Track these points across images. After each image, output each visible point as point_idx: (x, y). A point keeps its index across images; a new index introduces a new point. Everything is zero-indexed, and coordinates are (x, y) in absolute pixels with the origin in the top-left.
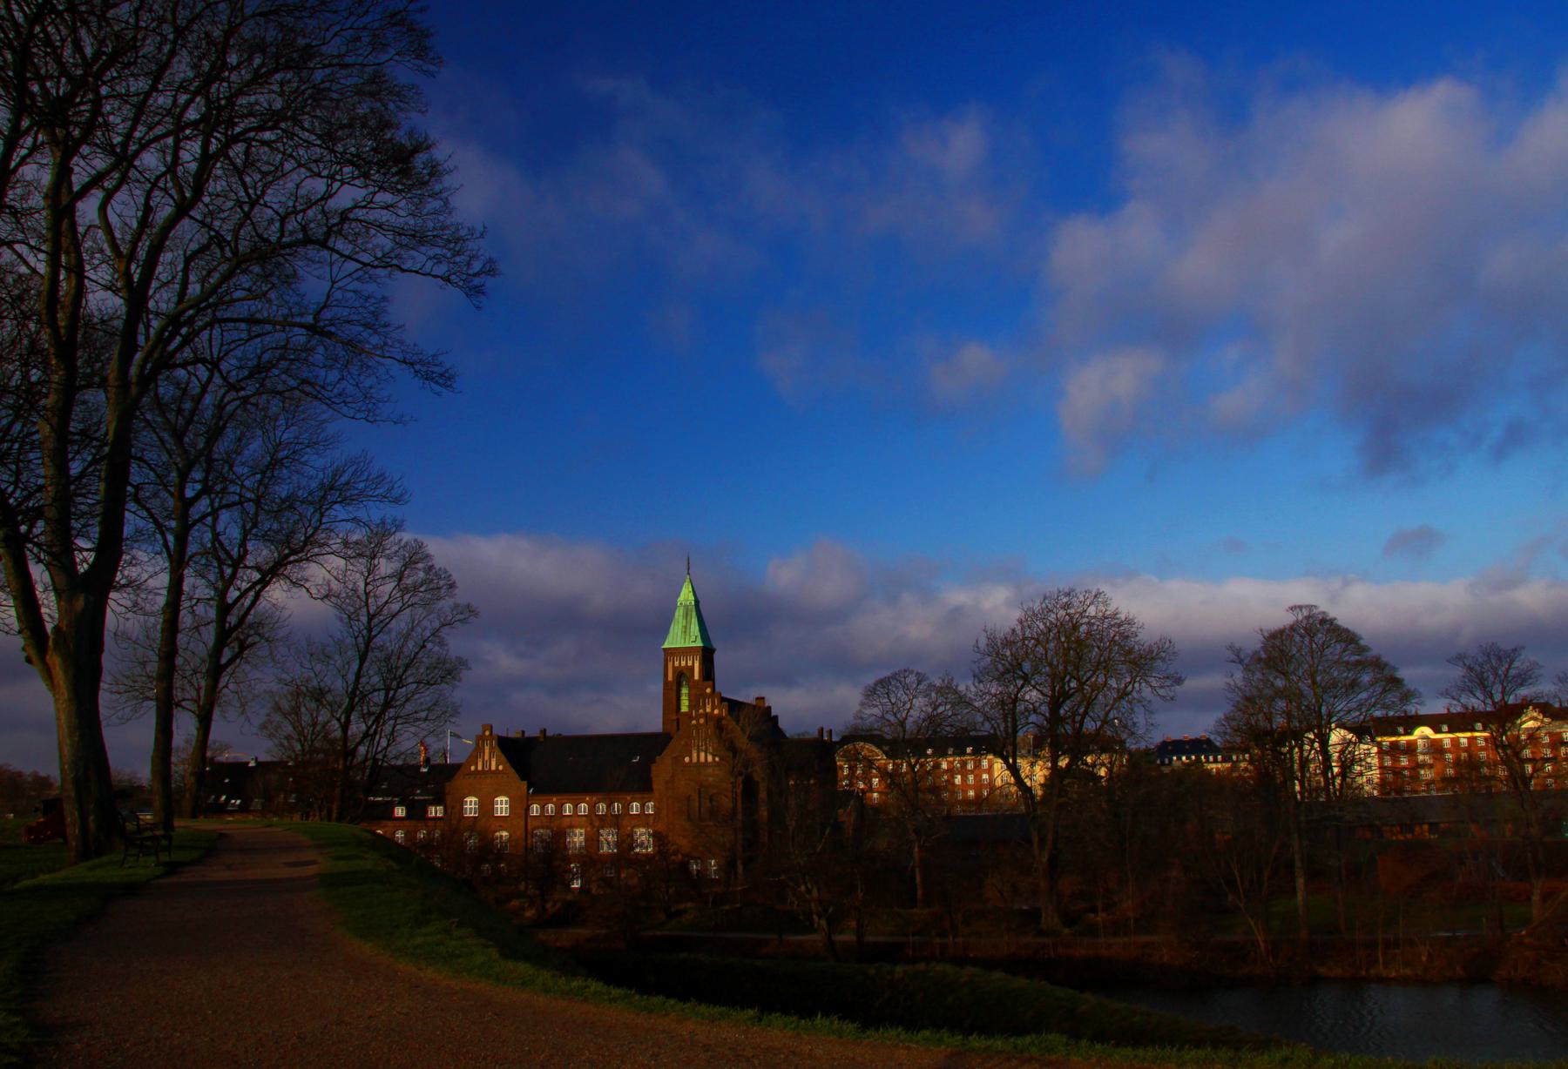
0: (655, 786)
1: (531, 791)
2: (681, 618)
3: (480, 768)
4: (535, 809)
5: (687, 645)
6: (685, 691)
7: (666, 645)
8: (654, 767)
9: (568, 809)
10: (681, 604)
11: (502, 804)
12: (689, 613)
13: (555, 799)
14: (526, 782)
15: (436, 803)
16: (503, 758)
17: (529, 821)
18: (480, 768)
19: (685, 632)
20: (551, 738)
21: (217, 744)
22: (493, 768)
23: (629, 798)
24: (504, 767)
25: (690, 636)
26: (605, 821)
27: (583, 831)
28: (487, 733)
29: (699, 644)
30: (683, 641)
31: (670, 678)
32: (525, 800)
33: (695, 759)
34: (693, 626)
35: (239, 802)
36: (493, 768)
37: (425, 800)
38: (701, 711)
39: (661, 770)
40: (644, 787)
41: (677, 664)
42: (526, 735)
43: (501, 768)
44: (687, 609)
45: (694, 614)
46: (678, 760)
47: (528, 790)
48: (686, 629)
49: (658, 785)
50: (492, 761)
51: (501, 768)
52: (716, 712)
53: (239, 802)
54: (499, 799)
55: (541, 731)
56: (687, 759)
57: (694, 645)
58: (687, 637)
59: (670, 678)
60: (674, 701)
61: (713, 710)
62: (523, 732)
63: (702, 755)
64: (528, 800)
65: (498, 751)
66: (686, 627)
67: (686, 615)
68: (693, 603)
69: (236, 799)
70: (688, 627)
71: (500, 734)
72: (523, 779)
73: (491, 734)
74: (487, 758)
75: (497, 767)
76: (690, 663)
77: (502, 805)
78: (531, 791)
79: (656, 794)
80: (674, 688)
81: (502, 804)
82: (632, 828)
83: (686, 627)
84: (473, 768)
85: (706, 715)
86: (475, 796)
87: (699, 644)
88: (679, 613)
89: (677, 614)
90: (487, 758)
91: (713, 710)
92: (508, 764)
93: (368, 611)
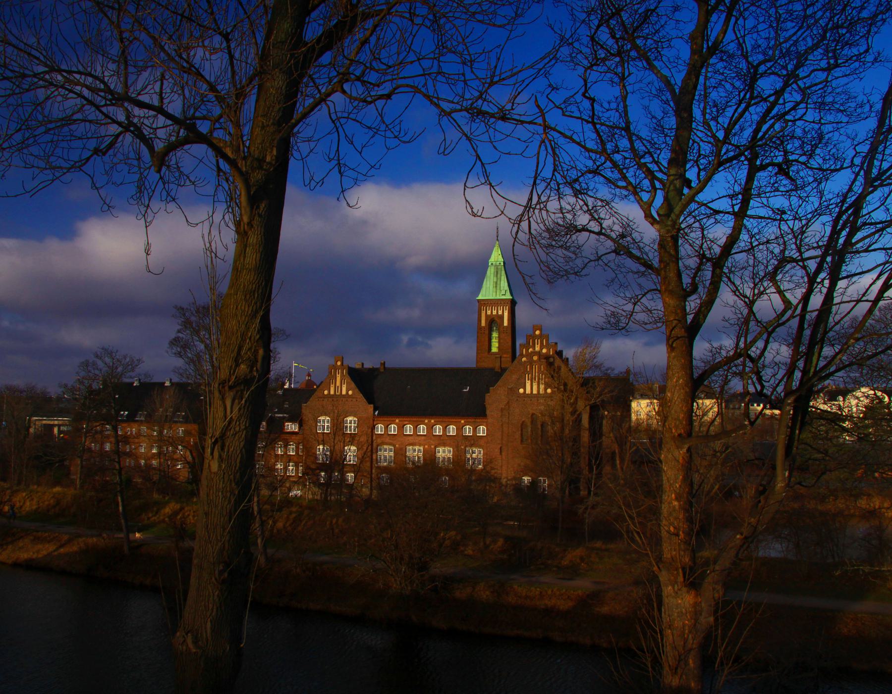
0: (488, 412)
1: (376, 413)
2: (492, 276)
3: (332, 392)
4: (380, 429)
5: (498, 297)
6: (495, 335)
7: (480, 297)
8: (487, 396)
9: (409, 429)
10: (492, 264)
11: (324, 427)
12: (499, 272)
13: (397, 421)
14: (372, 405)
15: (292, 420)
16: (353, 385)
17: (374, 438)
18: (332, 392)
19: (496, 287)
20: (389, 369)
21: (128, 360)
22: (344, 392)
23: (463, 422)
24: (353, 393)
25: (500, 290)
26: (443, 440)
27: (422, 448)
28: (339, 363)
29: (508, 296)
30: (494, 294)
31: (483, 323)
32: (371, 421)
33: (528, 391)
34: (502, 282)
35: (126, 413)
36: (344, 392)
37: (284, 418)
38: (530, 350)
39: (495, 399)
40: (477, 412)
41: (489, 312)
42: (365, 366)
43: (350, 393)
44: (497, 268)
45: (503, 272)
46: (513, 391)
47: (374, 413)
48: (496, 285)
49: (492, 410)
50: (342, 387)
51: (350, 393)
52: (544, 351)
53: (126, 413)
54: (322, 418)
55: (381, 363)
56: (521, 391)
57: (504, 297)
58: (498, 291)
59: (483, 323)
60: (487, 343)
61: (541, 349)
62: (363, 364)
63: (542, 387)
64: (374, 420)
65: (348, 379)
66: (496, 283)
67: (497, 273)
68: (502, 264)
69: (124, 411)
70: (498, 283)
71: (350, 366)
72: (370, 403)
73: (342, 364)
74: (338, 383)
75: (347, 393)
76: (500, 313)
77: (351, 423)
78: (376, 413)
79: (490, 420)
80: (487, 332)
81: (351, 423)
82: (435, 448)
83: (496, 283)
84: (326, 392)
85: (539, 354)
86: (355, 416)
87: (508, 296)
88: (491, 271)
89: (488, 272)
90: (338, 383)
91: (541, 349)
92: (357, 390)
93: (596, 152)
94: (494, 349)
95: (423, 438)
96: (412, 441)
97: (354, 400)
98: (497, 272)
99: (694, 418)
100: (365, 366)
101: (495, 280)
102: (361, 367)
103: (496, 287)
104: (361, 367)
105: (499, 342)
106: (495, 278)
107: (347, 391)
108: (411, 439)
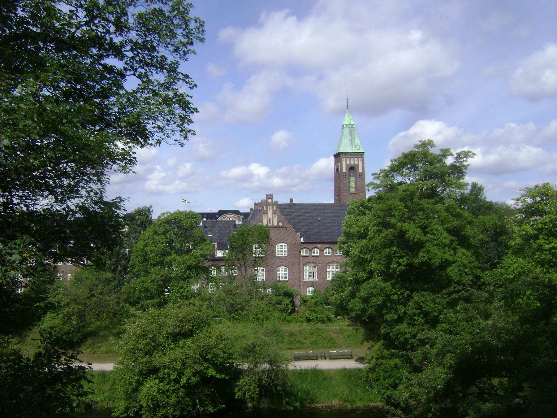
16: (283, 217)
19: (352, 143)
66: (352, 141)
70: (353, 140)
75: (278, 224)
94: (23, 156)
95: (340, 257)
96: (331, 260)
97: (285, 229)
98: (351, 132)
99: (231, 219)
100: (295, 202)
101: (350, 138)
102: (289, 202)
103: (352, 143)
104: (289, 202)
105: (356, 184)
106: (350, 137)
107: (278, 222)
108: (330, 259)
